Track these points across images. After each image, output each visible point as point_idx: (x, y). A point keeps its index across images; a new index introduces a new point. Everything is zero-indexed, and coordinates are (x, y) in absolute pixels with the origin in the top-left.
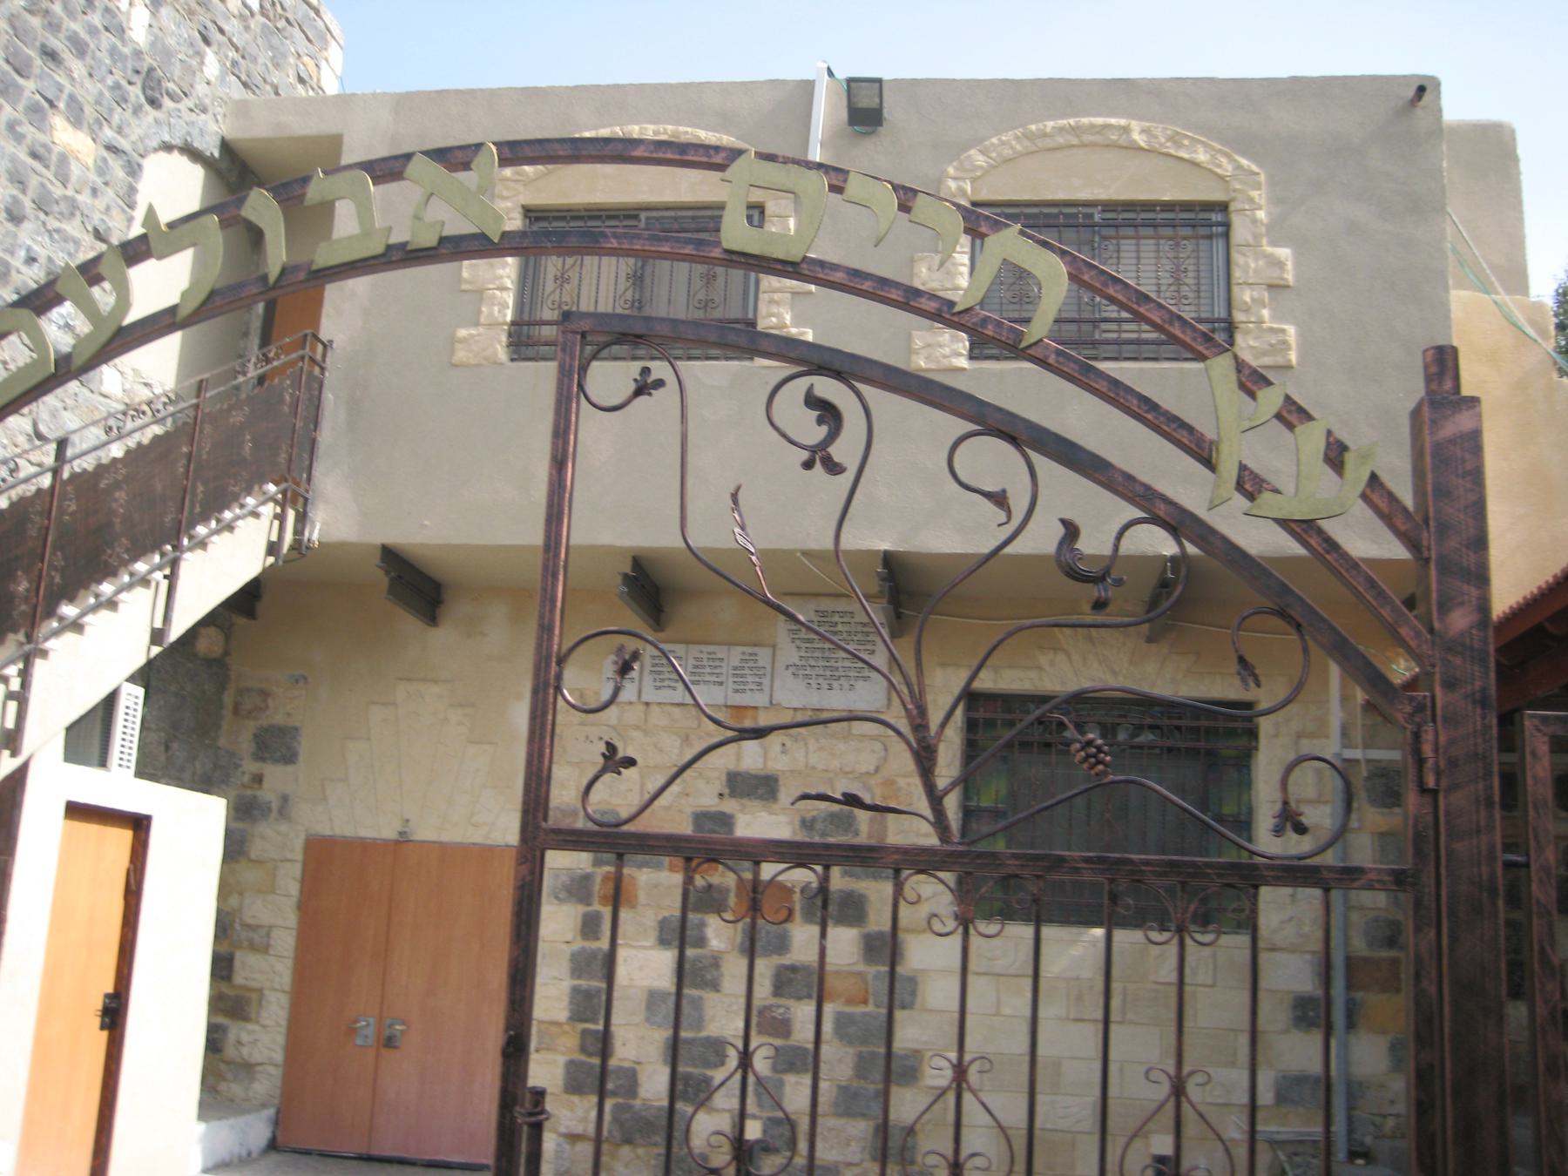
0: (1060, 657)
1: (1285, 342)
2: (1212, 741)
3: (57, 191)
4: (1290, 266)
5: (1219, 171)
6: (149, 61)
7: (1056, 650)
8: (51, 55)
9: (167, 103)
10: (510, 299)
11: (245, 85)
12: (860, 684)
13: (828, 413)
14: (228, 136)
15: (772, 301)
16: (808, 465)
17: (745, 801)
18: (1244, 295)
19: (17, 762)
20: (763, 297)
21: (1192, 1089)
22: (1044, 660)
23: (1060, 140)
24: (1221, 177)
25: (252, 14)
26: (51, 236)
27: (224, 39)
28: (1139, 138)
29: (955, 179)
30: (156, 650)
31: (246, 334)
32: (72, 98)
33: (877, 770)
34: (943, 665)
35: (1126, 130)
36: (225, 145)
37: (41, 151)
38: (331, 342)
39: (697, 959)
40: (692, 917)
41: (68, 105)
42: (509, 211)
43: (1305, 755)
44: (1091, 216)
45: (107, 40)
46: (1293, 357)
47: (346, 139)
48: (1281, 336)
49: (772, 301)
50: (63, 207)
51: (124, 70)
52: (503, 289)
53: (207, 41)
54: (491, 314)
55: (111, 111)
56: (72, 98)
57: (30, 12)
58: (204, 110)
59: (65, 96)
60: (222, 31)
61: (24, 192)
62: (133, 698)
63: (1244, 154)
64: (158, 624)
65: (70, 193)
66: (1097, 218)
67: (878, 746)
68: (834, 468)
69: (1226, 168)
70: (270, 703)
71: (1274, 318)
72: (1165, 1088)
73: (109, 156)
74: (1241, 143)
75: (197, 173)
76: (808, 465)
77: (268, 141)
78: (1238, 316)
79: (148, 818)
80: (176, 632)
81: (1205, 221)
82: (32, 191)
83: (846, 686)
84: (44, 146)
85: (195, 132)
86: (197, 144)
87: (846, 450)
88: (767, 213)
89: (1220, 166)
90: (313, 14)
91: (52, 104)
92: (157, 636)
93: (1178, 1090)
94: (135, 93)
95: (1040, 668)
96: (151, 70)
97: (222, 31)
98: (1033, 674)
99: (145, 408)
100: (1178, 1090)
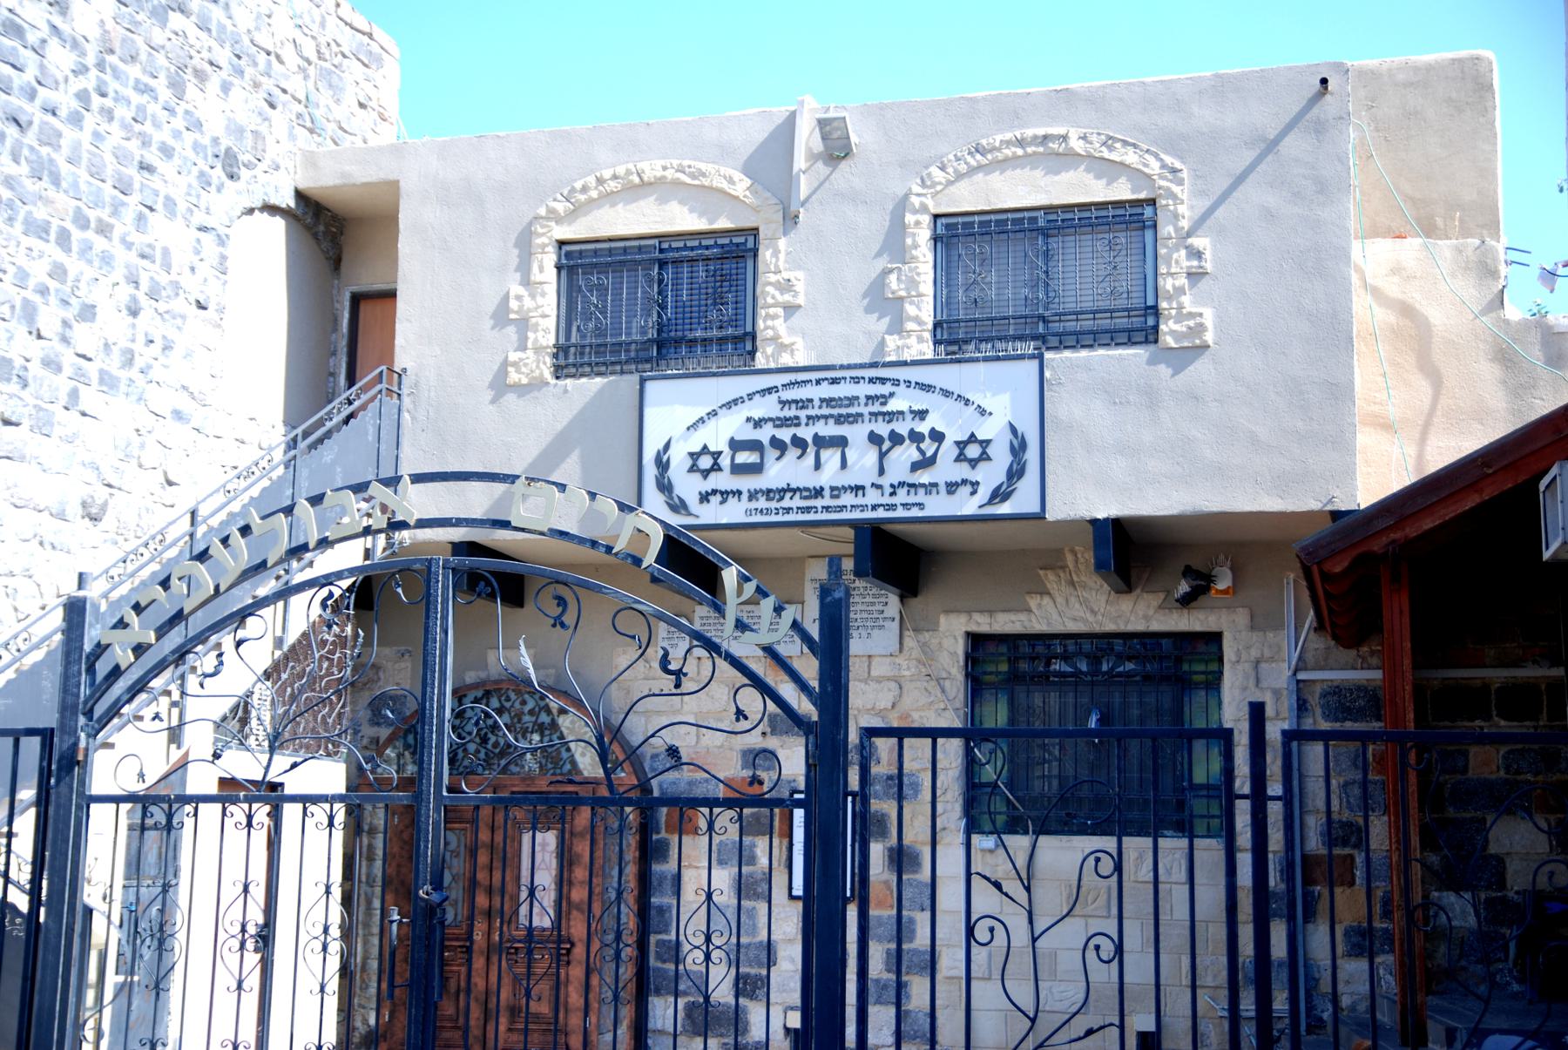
0: (1046, 600)
1: (1201, 325)
2: (1187, 662)
3: (163, 279)
4: (1208, 255)
5: (1146, 170)
6: (226, 142)
7: (1041, 594)
8: (145, 167)
9: (244, 173)
10: (551, 323)
11: (311, 131)
12: (876, 632)
13: (561, 601)
14: (301, 186)
15: (768, 316)
16: (554, 626)
17: (784, 737)
18: (1167, 284)
19: (183, 750)
20: (762, 312)
21: (715, 898)
22: (1033, 602)
23: (1008, 152)
24: (1149, 176)
25: (310, 63)
26: (163, 319)
27: (287, 97)
28: (1077, 145)
29: (918, 195)
30: (278, 653)
31: (334, 353)
32: (167, 198)
33: (893, 706)
34: (947, 612)
35: (1065, 138)
36: (300, 195)
37: (147, 251)
38: (404, 370)
39: (751, 875)
40: (747, 840)
41: (165, 205)
42: (544, 246)
43: (1263, 666)
44: (1035, 219)
45: (189, 137)
46: (1209, 337)
47: (402, 184)
48: (1198, 320)
49: (768, 316)
50: (170, 291)
51: (206, 158)
52: (545, 316)
53: (272, 106)
54: (536, 340)
55: (198, 196)
56: (167, 198)
57: (128, 139)
58: (277, 168)
59: (161, 200)
60: (284, 91)
61: (137, 288)
62: (264, 692)
63: (1167, 152)
64: (279, 633)
65: (173, 277)
66: (1041, 223)
67: (893, 685)
68: (563, 625)
69: (1154, 167)
70: (381, 674)
71: (1193, 303)
72: (704, 897)
73: (201, 235)
74: (1172, 143)
75: (279, 224)
76: (554, 626)
77: (335, 187)
78: (1163, 305)
79: (757, 229)
80: (292, 638)
81: (1135, 218)
82: (145, 285)
83: (864, 634)
84: (150, 246)
85: (271, 191)
86: (274, 201)
87: (569, 619)
88: (762, 235)
89: (1146, 165)
90: (366, 39)
91: (151, 209)
92: (279, 642)
93: (709, 896)
94: (218, 174)
95: (1029, 610)
96: (228, 150)
97: (284, 91)
98: (1023, 617)
99: (254, 469)
100: (709, 896)
